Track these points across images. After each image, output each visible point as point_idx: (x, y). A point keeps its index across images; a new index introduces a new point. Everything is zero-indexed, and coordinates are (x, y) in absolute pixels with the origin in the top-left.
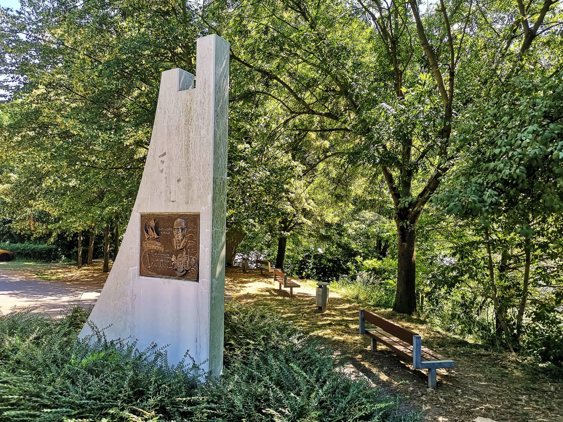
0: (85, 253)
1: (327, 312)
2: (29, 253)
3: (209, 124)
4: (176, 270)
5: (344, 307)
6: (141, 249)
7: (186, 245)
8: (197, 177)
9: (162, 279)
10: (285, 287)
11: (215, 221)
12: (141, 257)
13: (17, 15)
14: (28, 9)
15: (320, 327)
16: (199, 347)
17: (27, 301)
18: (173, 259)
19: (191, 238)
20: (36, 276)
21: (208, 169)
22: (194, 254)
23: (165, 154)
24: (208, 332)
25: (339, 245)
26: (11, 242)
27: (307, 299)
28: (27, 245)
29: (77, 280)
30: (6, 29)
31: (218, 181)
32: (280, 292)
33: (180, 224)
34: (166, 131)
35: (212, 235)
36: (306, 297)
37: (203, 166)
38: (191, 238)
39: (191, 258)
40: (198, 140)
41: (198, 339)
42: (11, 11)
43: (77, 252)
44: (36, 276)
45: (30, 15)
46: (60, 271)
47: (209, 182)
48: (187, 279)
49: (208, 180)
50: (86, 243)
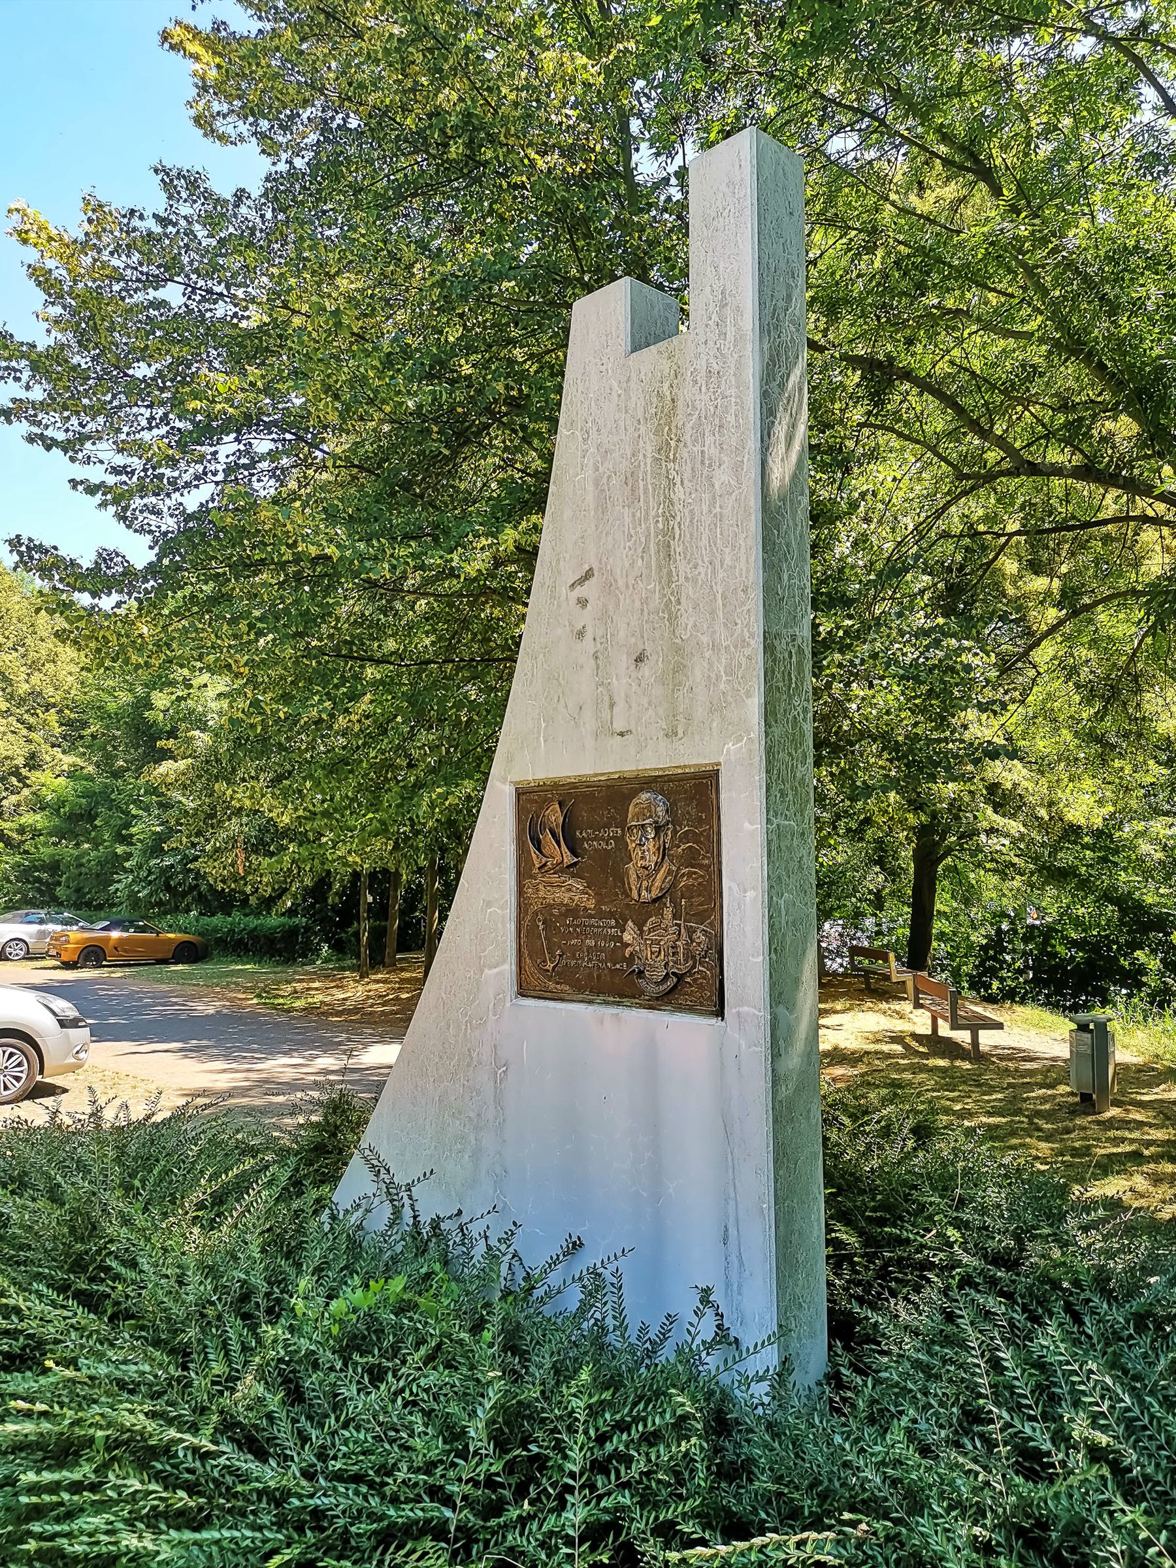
0: (378, 935)
1: (1113, 1112)
2: (242, 939)
3: (743, 443)
4: (641, 974)
5: (1166, 1096)
6: (519, 906)
7: (674, 885)
8: (705, 639)
9: (591, 1008)
10: (955, 1027)
11: (775, 792)
12: (519, 931)
13: (157, 229)
14: (185, 210)
15: (1106, 1167)
16: (734, 1258)
17: (224, 1071)
18: (627, 937)
19: (691, 859)
20: (255, 1001)
21: (743, 604)
22: (701, 917)
23: (589, 575)
24: (768, 1205)
25: (1108, 896)
26: (201, 914)
27: (1029, 1066)
28: (237, 920)
29: (356, 1010)
30: (129, 272)
31: (781, 645)
32: (936, 1044)
33: (648, 810)
34: (590, 498)
35: (769, 842)
36: (1024, 1059)
37: (724, 597)
38: (691, 859)
39: (691, 932)
40: (705, 508)
41: (732, 1231)
42: (141, 217)
43: (357, 935)
44: (255, 1001)
45: (190, 223)
46: (317, 985)
47: (747, 651)
48: (680, 1009)
49: (744, 643)
50: (380, 911)
